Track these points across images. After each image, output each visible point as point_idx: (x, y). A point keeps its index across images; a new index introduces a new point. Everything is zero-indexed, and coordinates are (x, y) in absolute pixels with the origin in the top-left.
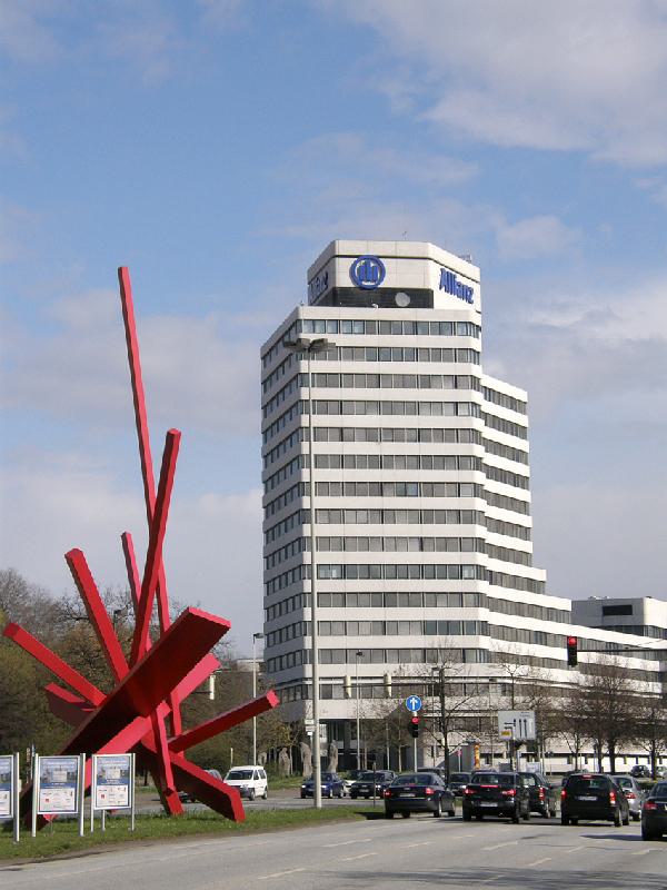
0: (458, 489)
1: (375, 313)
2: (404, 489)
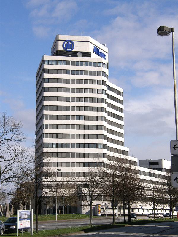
0: (97, 118)
1: (70, 58)
2: (78, 118)
